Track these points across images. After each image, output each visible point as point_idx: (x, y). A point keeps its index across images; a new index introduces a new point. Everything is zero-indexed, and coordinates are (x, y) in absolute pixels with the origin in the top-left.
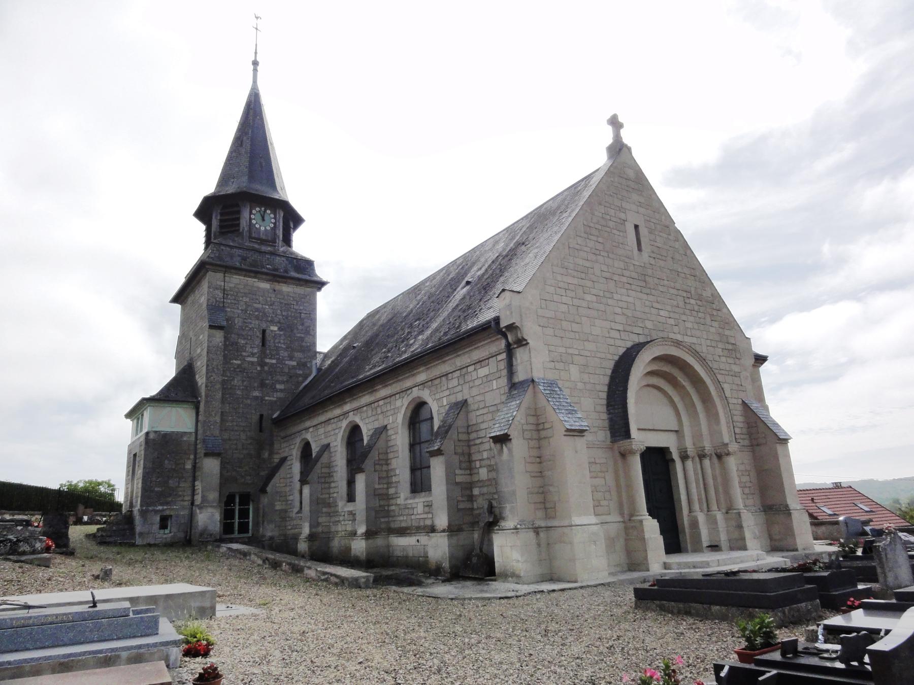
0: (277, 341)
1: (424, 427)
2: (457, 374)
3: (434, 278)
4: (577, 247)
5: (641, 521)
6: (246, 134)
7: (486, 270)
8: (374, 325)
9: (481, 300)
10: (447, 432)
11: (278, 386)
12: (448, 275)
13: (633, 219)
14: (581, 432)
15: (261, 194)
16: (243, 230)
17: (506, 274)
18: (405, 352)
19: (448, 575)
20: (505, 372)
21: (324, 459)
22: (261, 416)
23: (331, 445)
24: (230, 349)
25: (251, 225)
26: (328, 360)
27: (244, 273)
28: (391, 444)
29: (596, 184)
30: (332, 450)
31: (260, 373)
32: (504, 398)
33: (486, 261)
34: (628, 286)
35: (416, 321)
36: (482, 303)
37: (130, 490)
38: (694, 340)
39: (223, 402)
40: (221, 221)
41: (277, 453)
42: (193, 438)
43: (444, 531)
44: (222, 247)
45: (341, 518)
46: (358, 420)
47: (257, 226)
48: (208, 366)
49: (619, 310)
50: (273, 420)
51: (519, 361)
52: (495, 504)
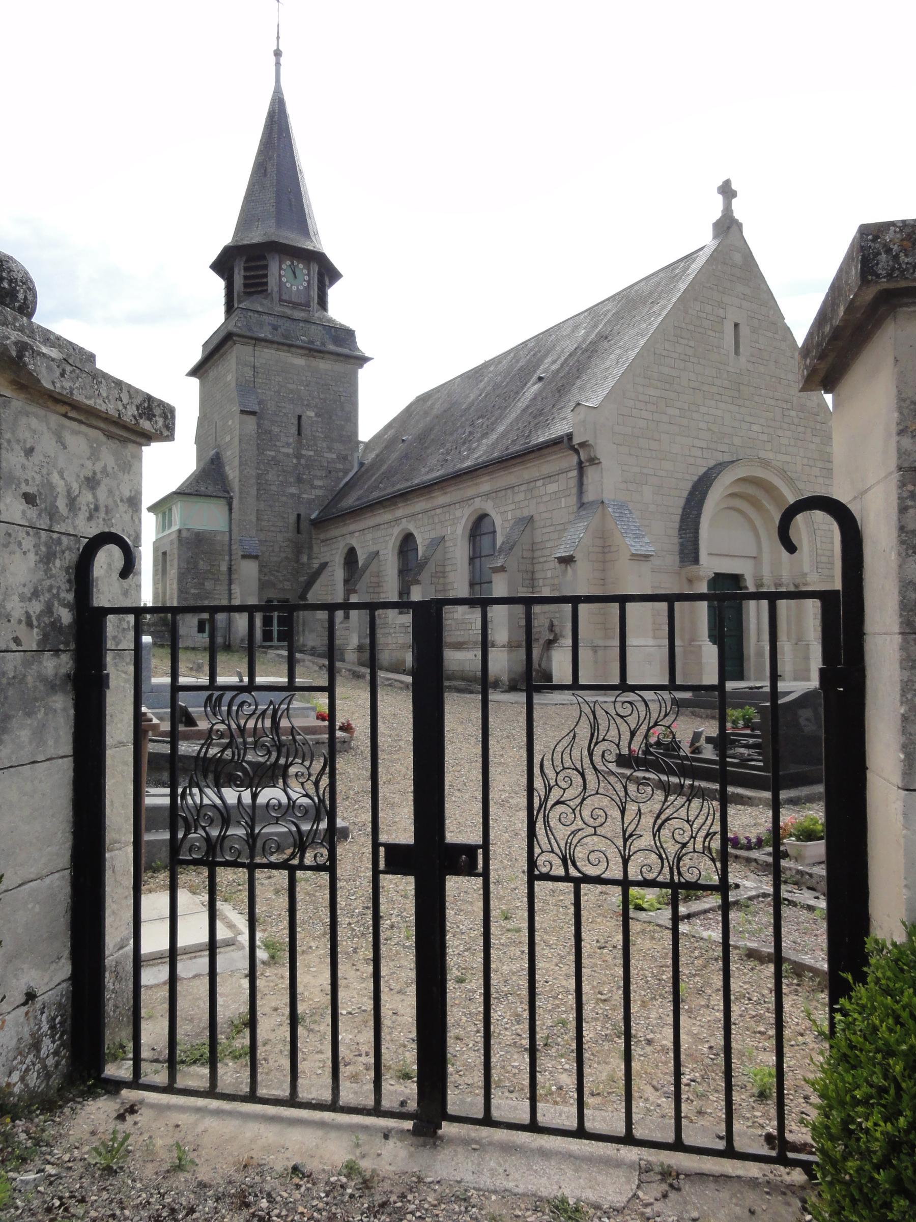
0: (314, 429)
1: (486, 541)
2: (523, 488)
3: (500, 362)
4: (665, 353)
5: (700, 646)
6: (270, 158)
7: (562, 365)
8: (426, 413)
9: (554, 406)
10: (511, 549)
11: (318, 483)
12: (517, 362)
13: (733, 315)
14: (646, 557)
15: (290, 243)
16: (272, 291)
17: (584, 377)
18: (467, 457)
19: (506, 688)
20: (574, 491)
21: (373, 568)
22: (299, 516)
23: (381, 553)
24: (264, 438)
25: (281, 284)
26: (371, 452)
27: (276, 346)
28: (448, 556)
29: (695, 273)
30: (382, 558)
31: (296, 466)
32: (572, 517)
33: (563, 351)
34: (718, 397)
35: (478, 418)
36: (555, 410)
37: (160, 591)
38: (788, 458)
39: (258, 499)
40: (245, 278)
41: (317, 558)
42: (227, 538)
43: (504, 646)
44: (250, 314)
45: (392, 631)
46: (412, 528)
47: (288, 285)
48: (240, 457)
49: (703, 425)
50: (311, 520)
51: (590, 480)
52: (556, 622)
